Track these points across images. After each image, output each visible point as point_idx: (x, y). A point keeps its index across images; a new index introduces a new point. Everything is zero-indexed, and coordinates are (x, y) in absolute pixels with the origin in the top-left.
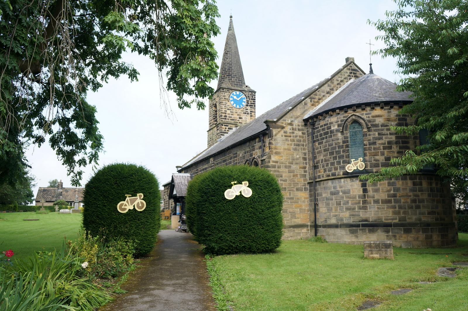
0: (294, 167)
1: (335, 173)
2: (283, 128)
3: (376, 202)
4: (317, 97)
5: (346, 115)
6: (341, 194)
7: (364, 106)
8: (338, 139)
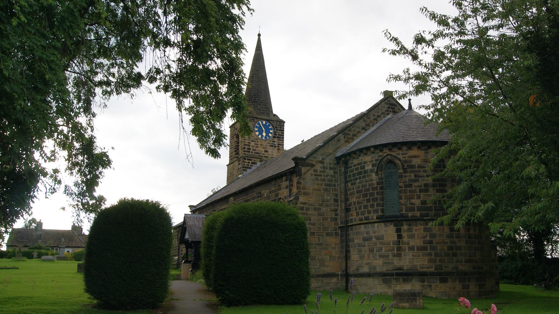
0: (323, 209)
2: (313, 166)
3: (411, 248)
4: (351, 133)
6: (374, 239)
8: (372, 180)
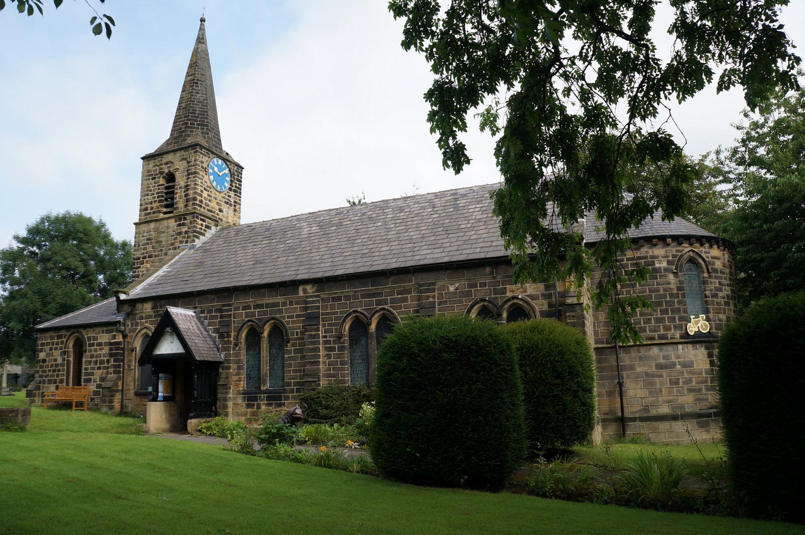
1: (667, 334)
5: (680, 248)
6: (678, 367)
7: (670, 240)
8: (669, 283)
